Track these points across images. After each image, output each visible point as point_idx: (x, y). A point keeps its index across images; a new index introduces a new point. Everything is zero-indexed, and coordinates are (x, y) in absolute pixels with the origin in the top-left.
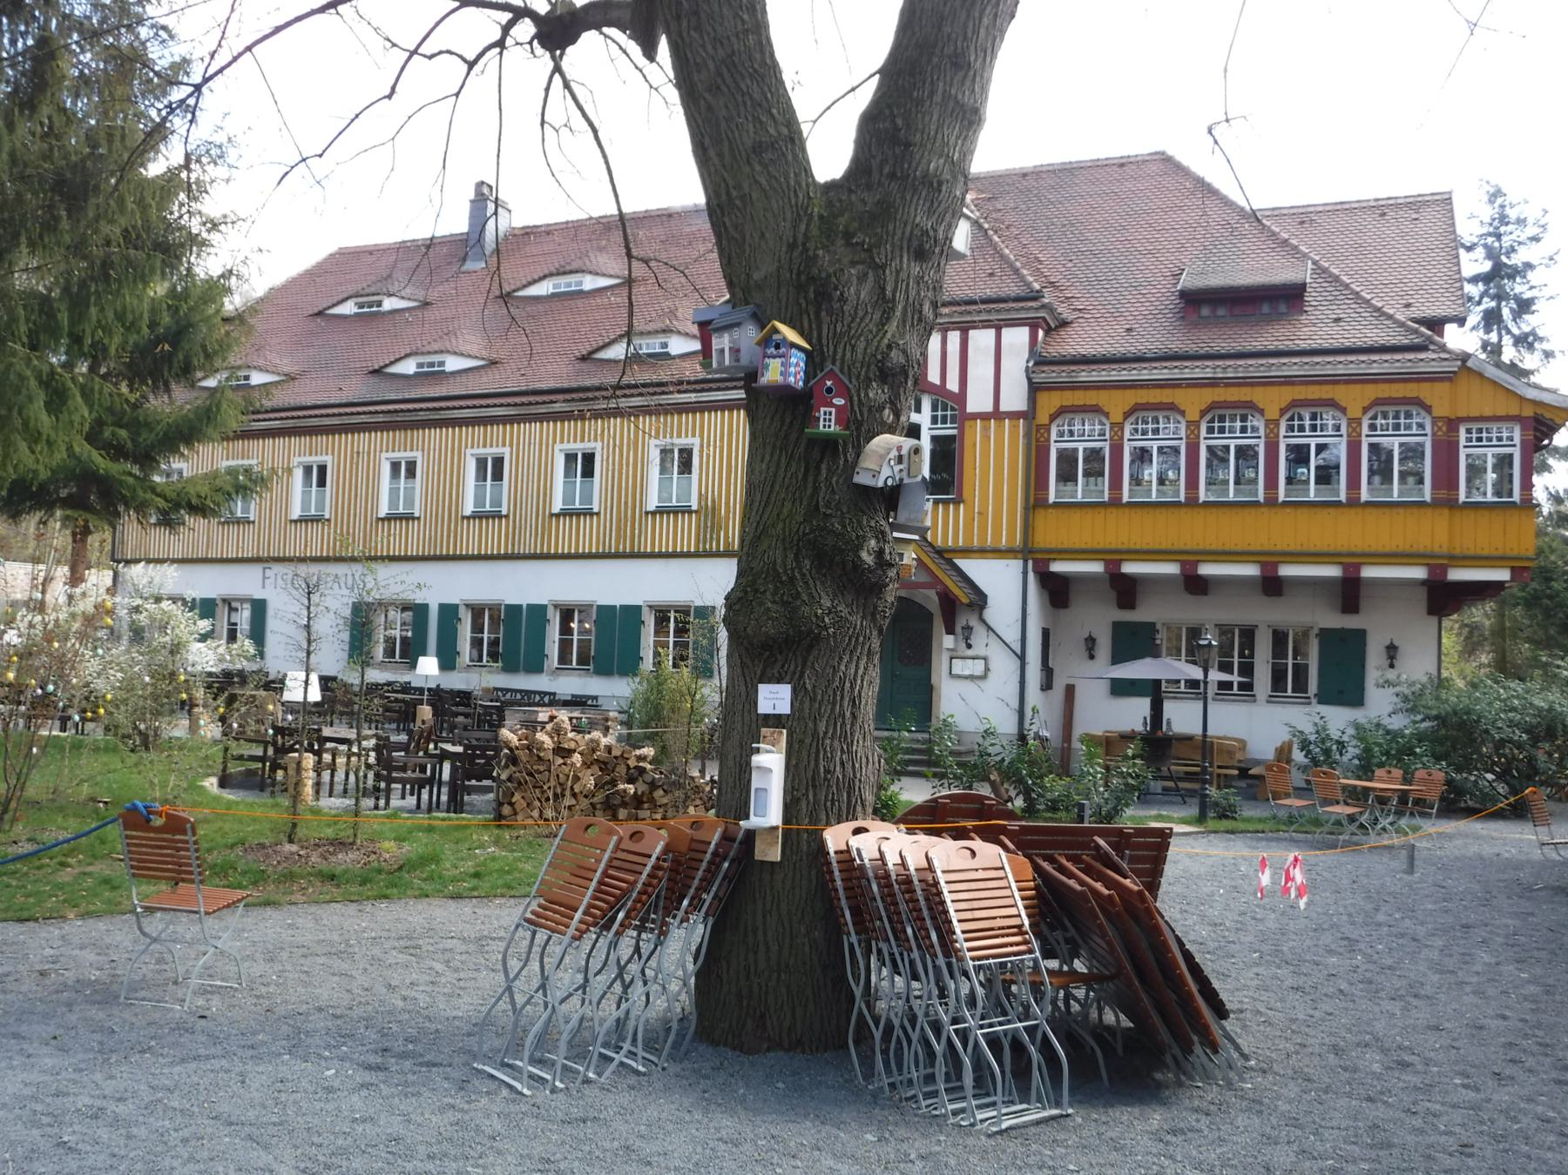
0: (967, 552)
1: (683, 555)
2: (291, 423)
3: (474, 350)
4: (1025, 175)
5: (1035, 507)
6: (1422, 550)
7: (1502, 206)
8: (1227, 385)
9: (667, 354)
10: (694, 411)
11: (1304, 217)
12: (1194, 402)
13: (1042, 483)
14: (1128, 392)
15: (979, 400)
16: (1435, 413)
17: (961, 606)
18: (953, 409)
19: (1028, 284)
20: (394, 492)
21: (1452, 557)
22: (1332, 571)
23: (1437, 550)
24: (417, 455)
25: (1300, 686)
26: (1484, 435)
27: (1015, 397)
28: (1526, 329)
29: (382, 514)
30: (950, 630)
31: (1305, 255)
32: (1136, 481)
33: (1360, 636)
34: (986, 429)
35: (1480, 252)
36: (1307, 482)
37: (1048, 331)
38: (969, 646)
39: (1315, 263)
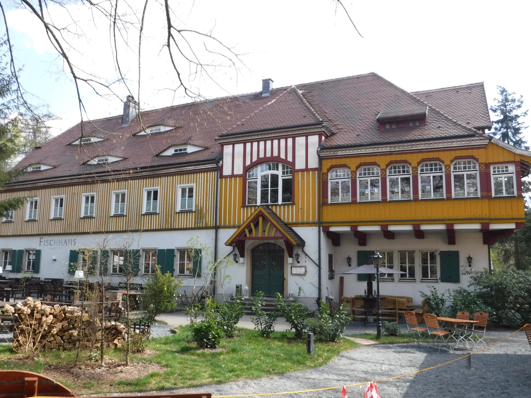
0: (297, 224)
1: (186, 229)
2: (51, 183)
3: (119, 154)
4: (322, 84)
5: (322, 205)
6: (478, 217)
7: (506, 95)
8: (396, 154)
9: (186, 153)
10: (194, 173)
11: (428, 94)
12: (383, 161)
13: (325, 196)
14: (358, 159)
15: (300, 165)
16: (480, 161)
17: (295, 246)
18: (291, 168)
19: (318, 119)
20: (86, 208)
21: (491, 219)
22: (442, 227)
23: (484, 217)
24: (95, 194)
25: (412, 274)
26: (500, 170)
27: (313, 163)
28: (518, 139)
29: (82, 216)
30: (291, 256)
31: (426, 105)
32: (363, 194)
33: (455, 255)
34: (303, 176)
35: (499, 112)
36: (430, 192)
37: (327, 137)
38: (299, 262)
39: (430, 107)
